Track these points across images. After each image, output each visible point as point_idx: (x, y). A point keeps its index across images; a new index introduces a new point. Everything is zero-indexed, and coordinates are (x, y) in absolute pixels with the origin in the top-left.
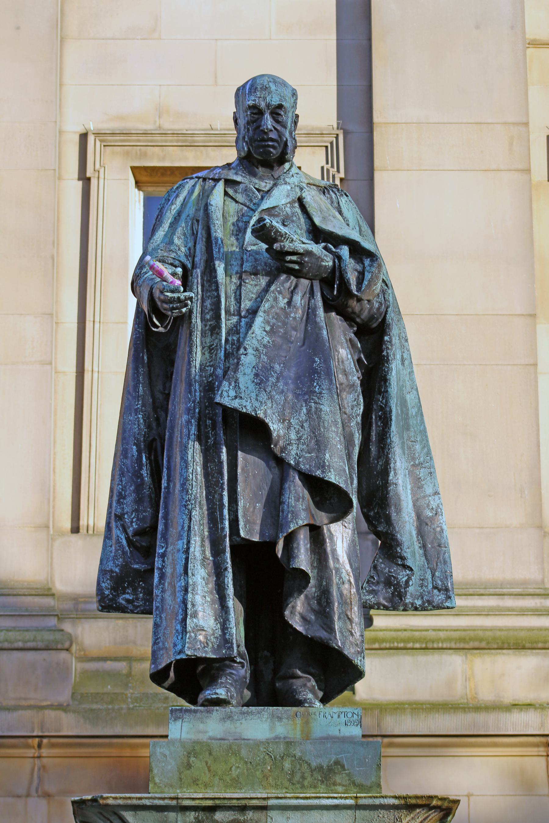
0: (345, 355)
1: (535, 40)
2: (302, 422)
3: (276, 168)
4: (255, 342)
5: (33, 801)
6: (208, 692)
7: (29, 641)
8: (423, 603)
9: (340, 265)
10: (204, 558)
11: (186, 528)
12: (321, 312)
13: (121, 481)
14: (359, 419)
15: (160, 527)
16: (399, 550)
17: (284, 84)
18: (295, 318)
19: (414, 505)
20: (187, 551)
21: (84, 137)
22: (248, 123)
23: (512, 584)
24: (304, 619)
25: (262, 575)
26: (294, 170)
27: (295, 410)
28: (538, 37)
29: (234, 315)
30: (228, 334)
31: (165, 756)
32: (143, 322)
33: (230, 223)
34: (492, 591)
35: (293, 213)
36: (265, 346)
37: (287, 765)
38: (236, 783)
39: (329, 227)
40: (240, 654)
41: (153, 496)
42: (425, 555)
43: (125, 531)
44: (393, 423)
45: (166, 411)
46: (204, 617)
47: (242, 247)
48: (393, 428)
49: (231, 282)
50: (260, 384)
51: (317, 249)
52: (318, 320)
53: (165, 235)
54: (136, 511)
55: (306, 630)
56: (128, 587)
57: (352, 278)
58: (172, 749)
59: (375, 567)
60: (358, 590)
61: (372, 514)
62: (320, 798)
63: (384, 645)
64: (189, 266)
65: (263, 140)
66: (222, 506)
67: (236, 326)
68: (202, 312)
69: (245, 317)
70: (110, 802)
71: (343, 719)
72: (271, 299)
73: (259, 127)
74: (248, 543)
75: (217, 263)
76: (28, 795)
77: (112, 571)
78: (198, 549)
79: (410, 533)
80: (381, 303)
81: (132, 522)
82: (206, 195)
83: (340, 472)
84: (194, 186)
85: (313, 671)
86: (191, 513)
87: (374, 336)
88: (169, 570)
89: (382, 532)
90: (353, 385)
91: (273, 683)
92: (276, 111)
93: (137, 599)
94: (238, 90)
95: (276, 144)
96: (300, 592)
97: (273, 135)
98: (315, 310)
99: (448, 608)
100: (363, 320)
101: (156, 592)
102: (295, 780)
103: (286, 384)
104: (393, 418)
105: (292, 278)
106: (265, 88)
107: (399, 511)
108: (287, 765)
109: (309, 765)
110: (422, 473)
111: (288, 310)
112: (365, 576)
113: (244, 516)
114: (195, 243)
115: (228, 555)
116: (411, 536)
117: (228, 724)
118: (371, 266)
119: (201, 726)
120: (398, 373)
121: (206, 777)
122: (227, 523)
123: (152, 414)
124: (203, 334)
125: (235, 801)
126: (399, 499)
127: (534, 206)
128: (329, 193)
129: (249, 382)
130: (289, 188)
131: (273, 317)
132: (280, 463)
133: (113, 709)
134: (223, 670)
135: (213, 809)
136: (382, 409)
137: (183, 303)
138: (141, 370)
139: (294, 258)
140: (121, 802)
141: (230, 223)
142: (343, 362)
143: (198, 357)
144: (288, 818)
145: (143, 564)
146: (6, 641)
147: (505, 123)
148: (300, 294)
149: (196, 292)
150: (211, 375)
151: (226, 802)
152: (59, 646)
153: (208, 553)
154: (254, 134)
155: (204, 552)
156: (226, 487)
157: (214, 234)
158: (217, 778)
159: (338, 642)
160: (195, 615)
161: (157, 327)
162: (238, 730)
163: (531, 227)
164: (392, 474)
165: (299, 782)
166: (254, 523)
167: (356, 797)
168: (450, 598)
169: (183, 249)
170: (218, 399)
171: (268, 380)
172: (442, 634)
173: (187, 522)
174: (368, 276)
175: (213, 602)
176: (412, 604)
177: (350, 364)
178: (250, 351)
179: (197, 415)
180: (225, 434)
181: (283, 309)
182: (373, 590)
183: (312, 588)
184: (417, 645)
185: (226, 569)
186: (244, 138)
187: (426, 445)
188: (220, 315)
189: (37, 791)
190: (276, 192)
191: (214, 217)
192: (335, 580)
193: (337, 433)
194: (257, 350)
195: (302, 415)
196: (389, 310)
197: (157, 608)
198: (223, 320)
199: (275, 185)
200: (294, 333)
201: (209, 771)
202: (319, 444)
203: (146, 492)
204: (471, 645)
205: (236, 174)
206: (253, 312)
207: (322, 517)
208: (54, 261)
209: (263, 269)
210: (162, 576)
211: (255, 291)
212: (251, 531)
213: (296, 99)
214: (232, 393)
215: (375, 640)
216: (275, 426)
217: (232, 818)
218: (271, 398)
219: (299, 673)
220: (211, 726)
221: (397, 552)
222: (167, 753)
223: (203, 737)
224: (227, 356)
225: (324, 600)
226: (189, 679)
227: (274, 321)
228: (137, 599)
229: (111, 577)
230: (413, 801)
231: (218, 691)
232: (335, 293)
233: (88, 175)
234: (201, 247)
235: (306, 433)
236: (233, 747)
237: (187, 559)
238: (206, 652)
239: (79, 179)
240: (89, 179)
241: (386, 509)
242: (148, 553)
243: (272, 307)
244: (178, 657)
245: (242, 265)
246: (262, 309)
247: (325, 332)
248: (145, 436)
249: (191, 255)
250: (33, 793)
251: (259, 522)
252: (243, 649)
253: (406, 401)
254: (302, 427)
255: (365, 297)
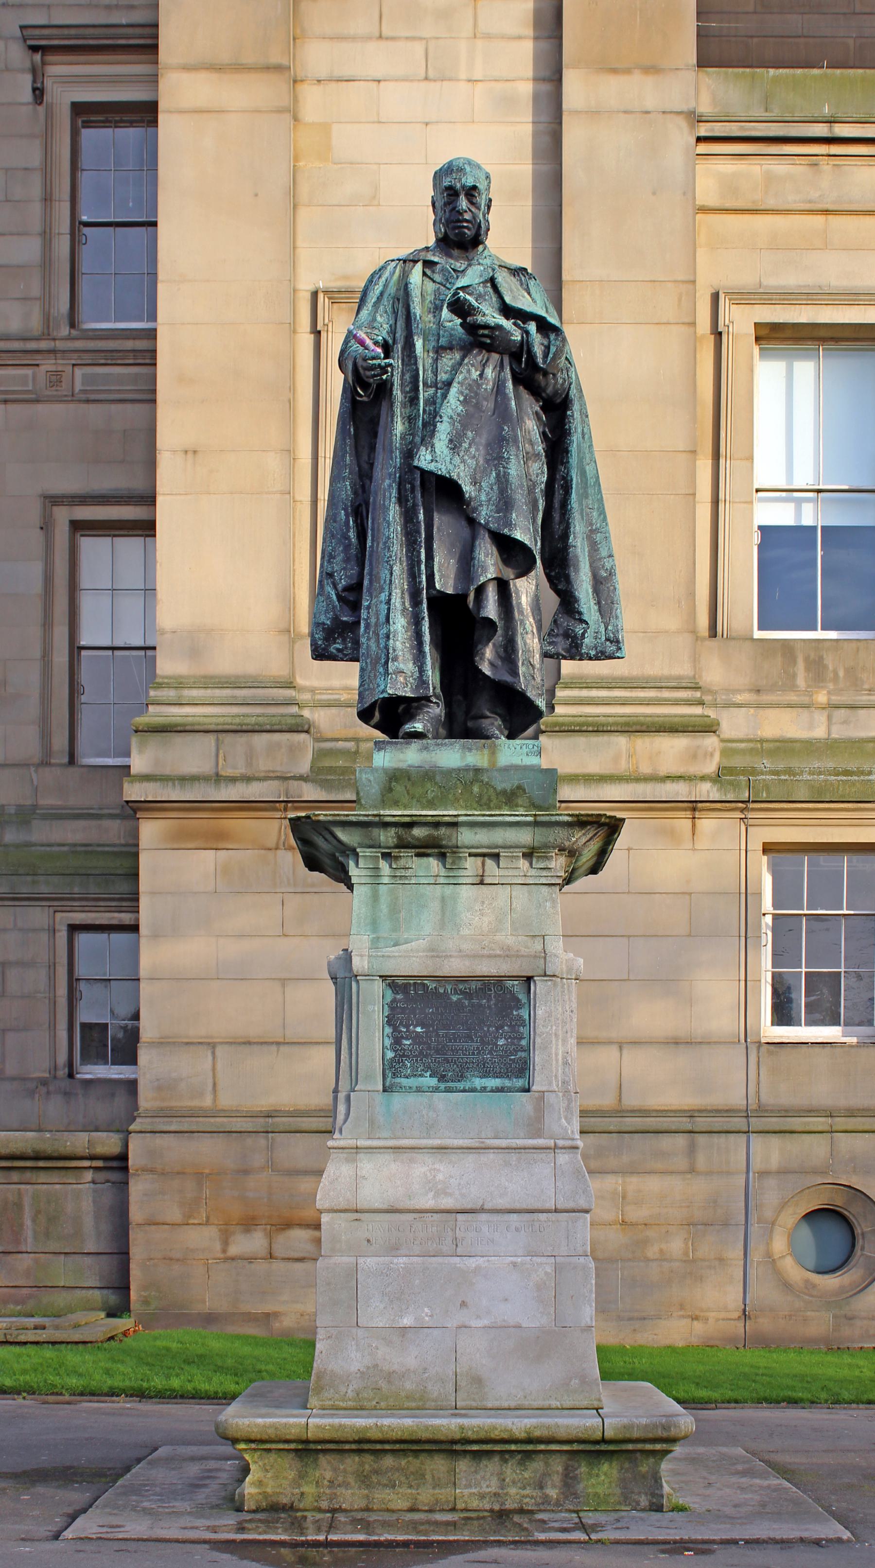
0: (531, 427)
1: (703, 206)
2: (491, 485)
3: (470, 250)
4: (449, 410)
5: (281, 853)
6: (407, 726)
7: (275, 725)
8: (597, 653)
9: (527, 340)
10: (404, 609)
11: (388, 582)
12: (510, 385)
13: (331, 543)
14: (543, 486)
15: (366, 582)
16: (576, 605)
17: (478, 167)
18: (486, 390)
19: (591, 566)
20: (388, 602)
21: (315, 295)
22: (445, 204)
23: (669, 678)
24: (492, 664)
25: (455, 625)
26: (486, 253)
27: (485, 472)
28: (706, 204)
29: (431, 387)
30: (425, 404)
31: (370, 781)
32: (350, 394)
33: (427, 302)
34: (652, 685)
35: (485, 293)
36: (459, 415)
37: (476, 789)
38: (431, 805)
39: (519, 305)
40: (435, 695)
41: (360, 555)
42: (600, 611)
43: (335, 586)
44: (573, 490)
45: (371, 478)
46: (404, 663)
47: (439, 324)
48: (574, 495)
49: (428, 356)
50: (454, 449)
51: (507, 324)
52: (507, 391)
53: (369, 314)
54: (344, 569)
55: (494, 674)
56: (338, 638)
57: (538, 350)
58: (376, 775)
59: (555, 621)
60: (539, 640)
61: (553, 574)
62: (503, 815)
63: (563, 728)
64: (391, 342)
65: (459, 221)
66: (419, 562)
67: (433, 398)
68: (402, 385)
69: (441, 389)
70: (322, 818)
71: (525, 750)
72: (464, 371)
73: (454, 209)
74: (443, 595)
75: (415, 338)
76: (277, 848)
77: (324, 624)
78: (398, 600)
79: (587, 591)
80: (564, 379)
81: (341, 579)
82: (405, 275)
83: (525, 532)
84: (395, 267)
85: (499, 711)
86: (391, 567)
87: (557, 411)
88: (373, 620)
89: (561, 590)
90: (538, 455)
91: (465, 723)
92: (471, 192)
93: (346, 648)
94: (436, 173)
95: (470, 225)
96: (489, 640)
97: (467, 216)
98: (504, 381)
99: (619, 658)
100: (547, 395)
101: (363, 640)
102: (483, 803)
103: (477, 450)
104: (574, 486)
105: (484, 352)
106: (461, 170)
107: (577, 570)
108: (476, 789)
109: (495, 789)
110: (598, 537)
111: (480, 382)
112: (546, 629)
113: (440, 570)
114: (396, 321)
115: (425, 605)
116: (588, 593)
117: (425, 754)
118: (556, 340)
119: (401, 756)
120: (579, 446)
121: (405, 799)
122: (424, 577)
123: (358, 481)
124: (404, 405)
125: (429, 818)
126: (578, 561)
127: (698, 356)
128: (519, 275)
129: (444, 447)
130: (482, 268)
131: (466, 388)
132: (472, 522)
133: (344, 779)
134: (421, 709)
135: (410, 825)
136: (564, 478)
137: (384, 369)
138: (348, 441)
139: (486, 332)
140: (330, 818)
141: (427, 302)
142: (529, 432)
143: (400, 427)
144: (476, 833)
145: (351, 616)
146: (257, 724)
147: (675, 281)
148: (491, 367)
149: (396, 361)
150: (410, 443)
151: (422, 818)
152: (300, 729)
153: (407, 604)
154: (450, 216)
155: (404, 603)
156: (423, 545)
157: (413, 311)
158: (415, 800)
159: (523, 684)
160: (395, 659)
161: (361, 396)
162: (433, 760)
163: (695, 375)
164: (572, 537)
165: (486, 804)
166: (448, 577)
167: (535, 815)
168: (620, 649)
169: (385, 326)
170: (416, 463)
171: (461, 445)
172: (610, 720)
173: (388, 576)
174: (553, 349)
175: (412, 647)
176: (587, 654)
177: (536, 436)
178: (445, 419)
179: (397, 480)
180: (422, 496)
181: (476, 381)
182: (553, 642)
183: (499, 637)
184: (590, 729)
185: (423, 618)
186: (441, 219)
187: (602, 512)
188: (418, 387)
189: (284, 845)
190: (470, 272)
191: (413, 294)
192: (520, 630)
193: (522, 495)
194: (451, 418)
195: (492, 478)
196: (572, 386)
197: (363, 654)
198: (421, 391)
199: (470, 265)
200: (485, 403)
201: (408, 794)
202: (505, 504)
203: (353, 551)
204: (634, 728)
205: (434, 255)
206: (448, 384)
207: (508, 573)
208: (292, 404)
209: (458, 344)
210: (367, 626)
211: (450, 364)
212: (446, 583)
213: (490, 182)
214: (429, 457)
215: (556, 724)
216: (468, 488)
217: (427, 833)
218: (463, 461)
219: (488, 714)
220: (411, 756)
221: (575, 608)
222: (372, 778)
223: (403, 765)
224: (425, 425)
225: (510, 648)
226: (389, 716)
227: (467, 391)
228: (346, 648)
229: (324, 629)
230: (585, 819)
231: (416, 725)
232: (523, 366)
233: (319, 329)
234: (401, 324)
235: (494, 496)
236: (428, 775)
237: (389, 609)
238: (405, 692)
239: (311, 333)
240: (319, 332)
241: (565, 569)
242: (355, 606)
243: (466, 378)
244: (381, 696)
245: (438, 340)
246: (456, 380)
247: (513, 403)
248: (352, 501)
249: (393, 332)
250: (281, 847)
251: (452, 576)
252: (438, 690)
253: (585, 472)
254: (492, 489)
255: (550, 370)
